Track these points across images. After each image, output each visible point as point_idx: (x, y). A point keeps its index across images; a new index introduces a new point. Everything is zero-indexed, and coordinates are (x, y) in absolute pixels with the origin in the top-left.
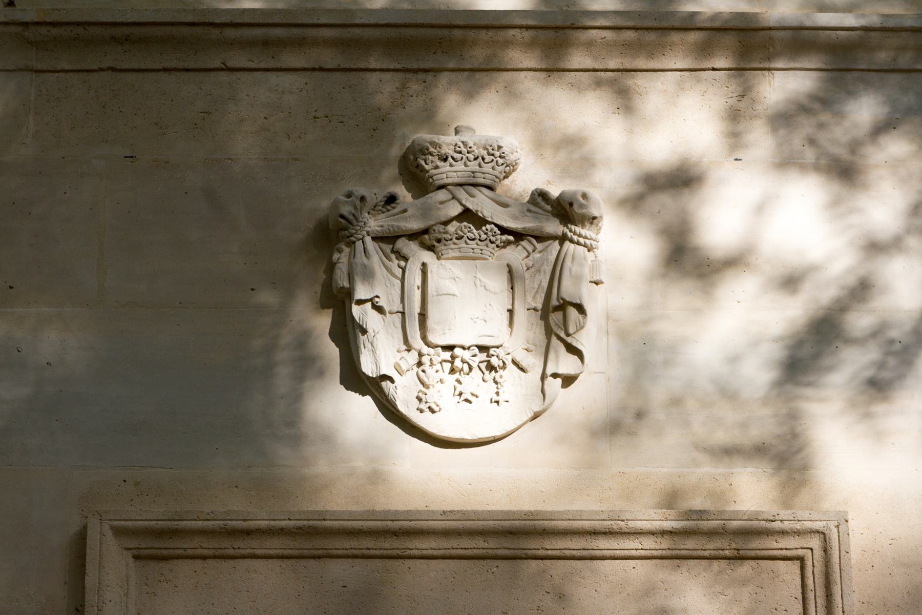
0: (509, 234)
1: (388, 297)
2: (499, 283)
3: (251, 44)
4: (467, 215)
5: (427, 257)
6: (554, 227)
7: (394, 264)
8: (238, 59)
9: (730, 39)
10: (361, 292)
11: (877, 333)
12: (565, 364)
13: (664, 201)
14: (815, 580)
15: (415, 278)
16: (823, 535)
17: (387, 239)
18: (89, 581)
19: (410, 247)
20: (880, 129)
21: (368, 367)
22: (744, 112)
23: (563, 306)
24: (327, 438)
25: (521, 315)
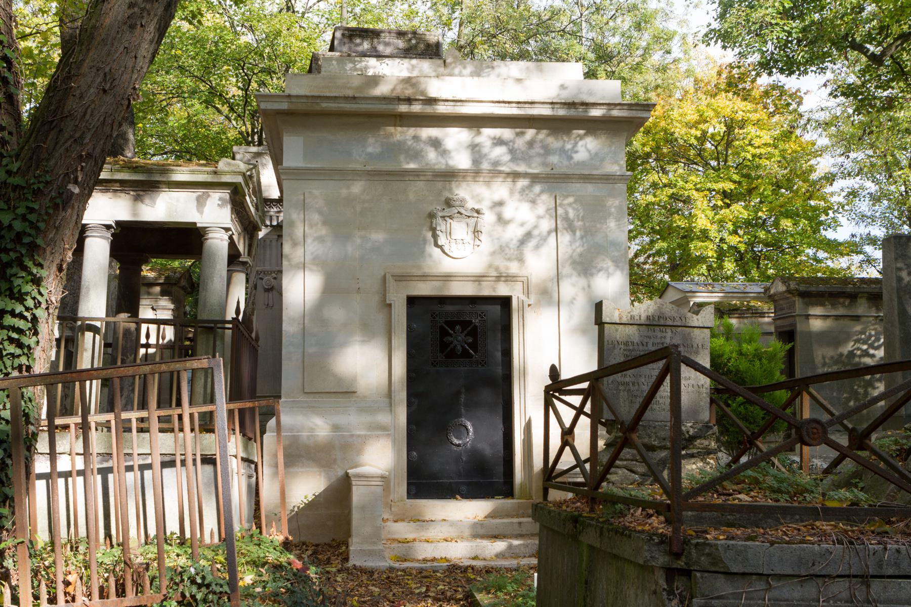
0: (896, 472)
1: (443, 228)
2: (465, 226)
3: (415, 175)
4: (459, 213)
5: (451, 221)
6: (476, 215)
7: (444, 222)
8: (411, 178)
9: (512, 175)
10: (438, 229)
11: (539, 235)
12: (478, 242)
13: (498, 209)
14: (525, 286)
15: (448, 225)
16: (527, 277)
17: (443, 217)
18: (387, 285)
19: (447, 219)
20: (542, 192)
21: (440, 243)
22: (527, 194)
23: (478, 232)
24: (430, 256)
25: (469, 233)
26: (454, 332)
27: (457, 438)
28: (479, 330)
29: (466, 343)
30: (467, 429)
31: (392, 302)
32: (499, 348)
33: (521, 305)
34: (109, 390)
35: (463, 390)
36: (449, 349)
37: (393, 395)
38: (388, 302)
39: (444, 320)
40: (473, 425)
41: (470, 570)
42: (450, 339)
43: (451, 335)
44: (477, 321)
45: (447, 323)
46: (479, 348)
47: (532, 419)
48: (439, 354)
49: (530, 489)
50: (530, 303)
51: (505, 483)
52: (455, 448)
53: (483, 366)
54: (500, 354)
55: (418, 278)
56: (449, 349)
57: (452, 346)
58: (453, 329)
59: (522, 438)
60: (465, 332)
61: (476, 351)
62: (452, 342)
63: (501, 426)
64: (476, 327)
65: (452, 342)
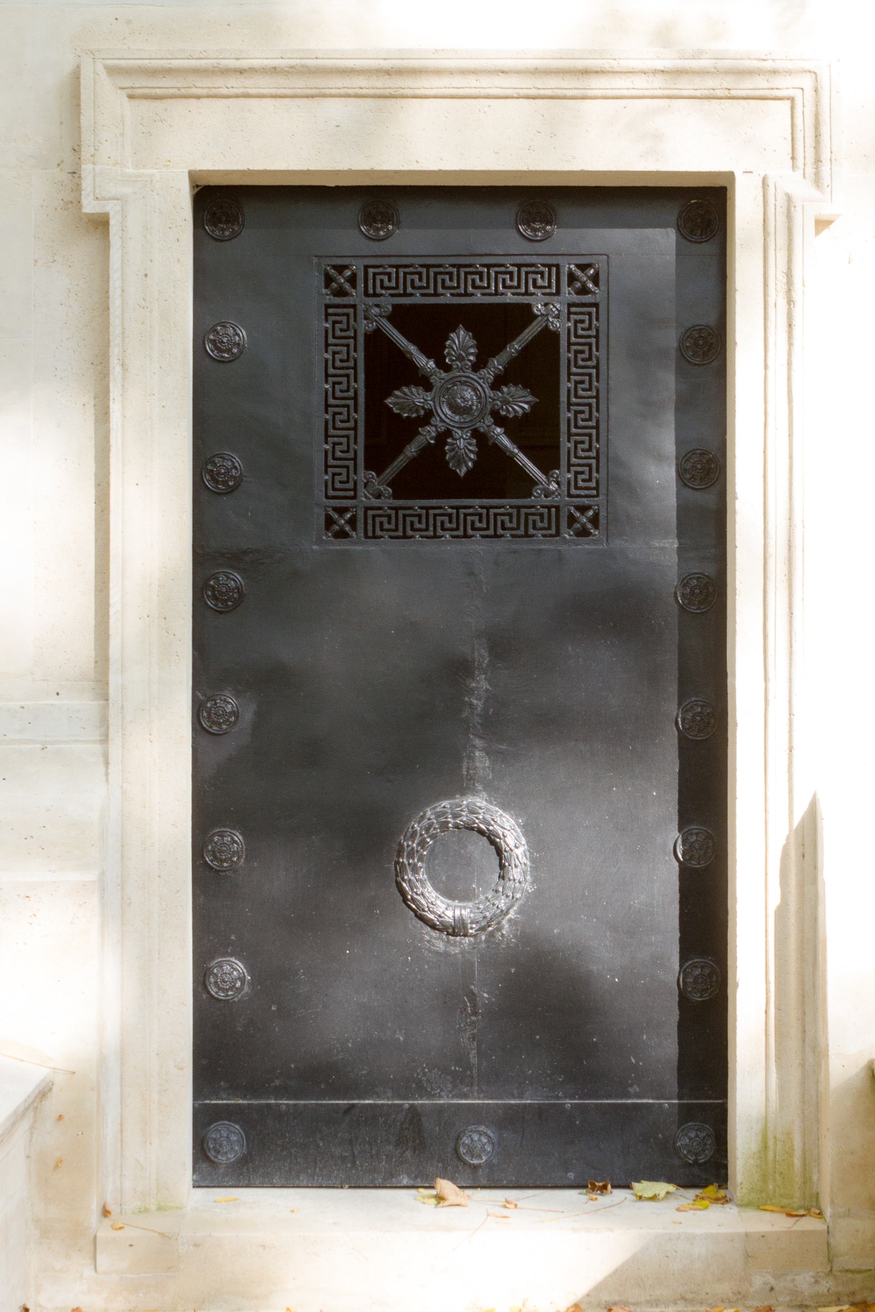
14: (804, 122)
18: (86, 120)
26: (442, 365)
27: (449, 893)
28: (565, 354)
29: (500, 420)
30: (492, 839)
31: (112, 209)
32: (667, 442)
33: (777, 220)
34: (80, 208)
35: (481, 655)
36: (412, 450)
37: (114, 679)
38: (90, 206)
39: (388, 303)
40: (529, 830)
41: (516, 1095)
42: (418, 397)
43: (426, 384)
44: (558, 305)
45: (400, 315)
46: (565, 445)
47: (819, 797)
48: (362, 475)
49: (810, 1161)
50: (826, 212)
51: (686, 1114)
52: (439, 942)
53: (583, 533)
54: (670, 472)
55: (265, 84)
56: (412, 450)
57: (428, 434)
58: (435, 351)
59: (775, 900)
60: (497, 364)
61: (548, 463)
62: (428, 416)
63: (672, 834)
64: (549, 338)
65: (428, 416)
